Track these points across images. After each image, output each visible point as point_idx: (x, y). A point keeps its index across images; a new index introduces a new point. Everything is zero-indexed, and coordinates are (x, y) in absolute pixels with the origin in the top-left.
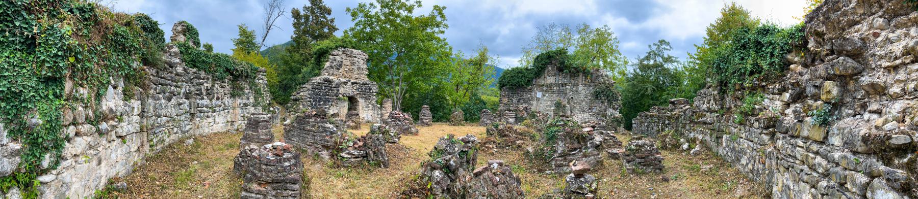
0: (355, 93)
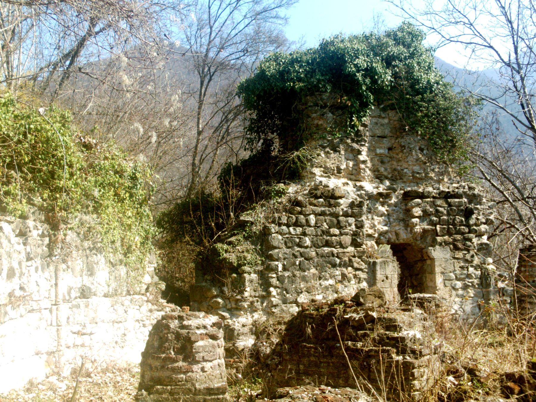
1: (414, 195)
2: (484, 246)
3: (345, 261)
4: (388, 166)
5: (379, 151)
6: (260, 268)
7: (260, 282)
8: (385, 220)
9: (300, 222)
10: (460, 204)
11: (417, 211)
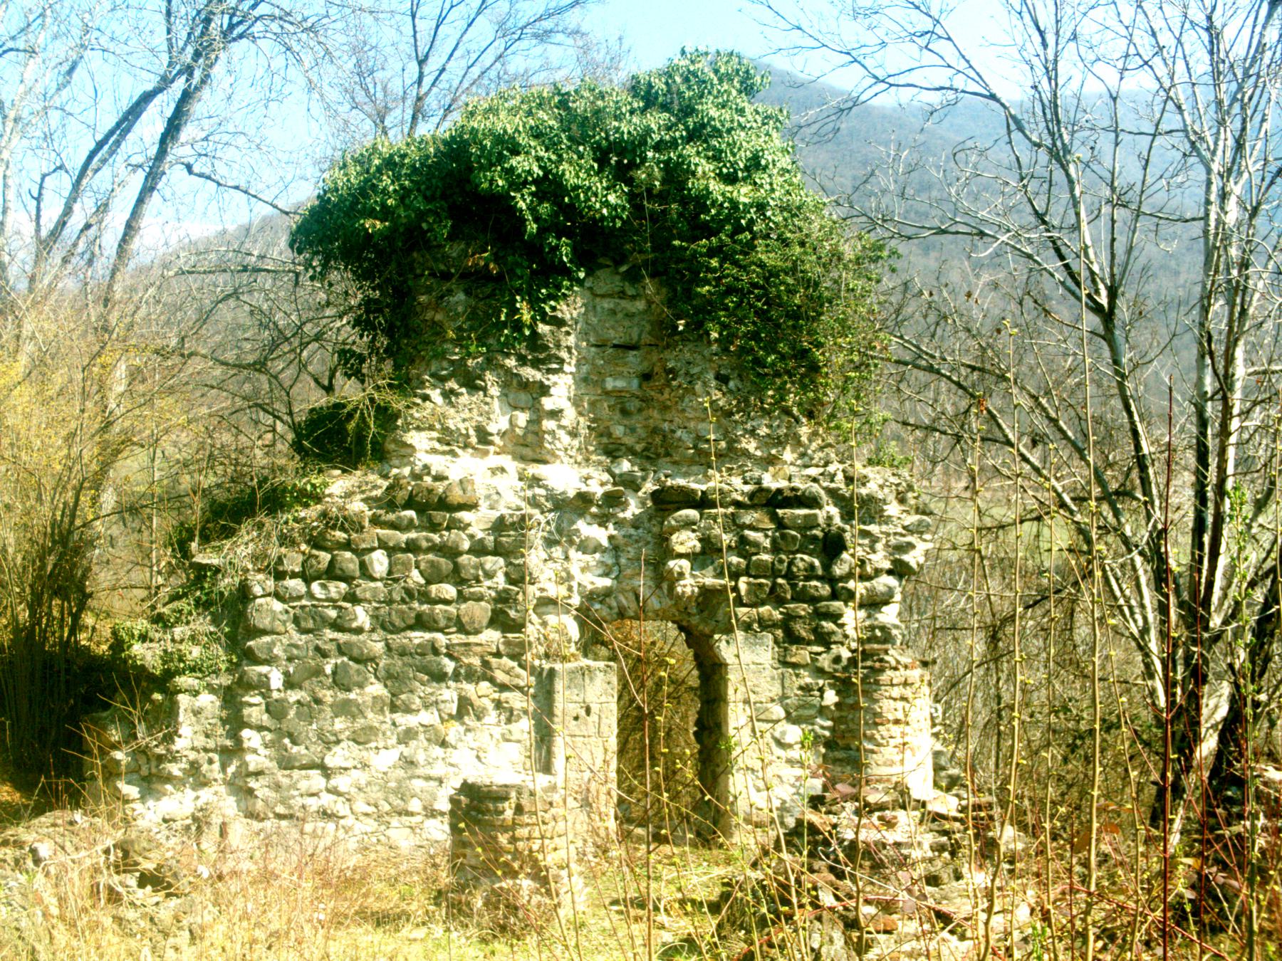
1: (675, 498)
2: (878, 633)
3: (469, 666)
4: (637, 422)
5: (610, 384)
6: (225, 680)
7: (224, 714)
8: (602, 563)
9: (341, 569)
10: (810, 523)
11: (685, 541)
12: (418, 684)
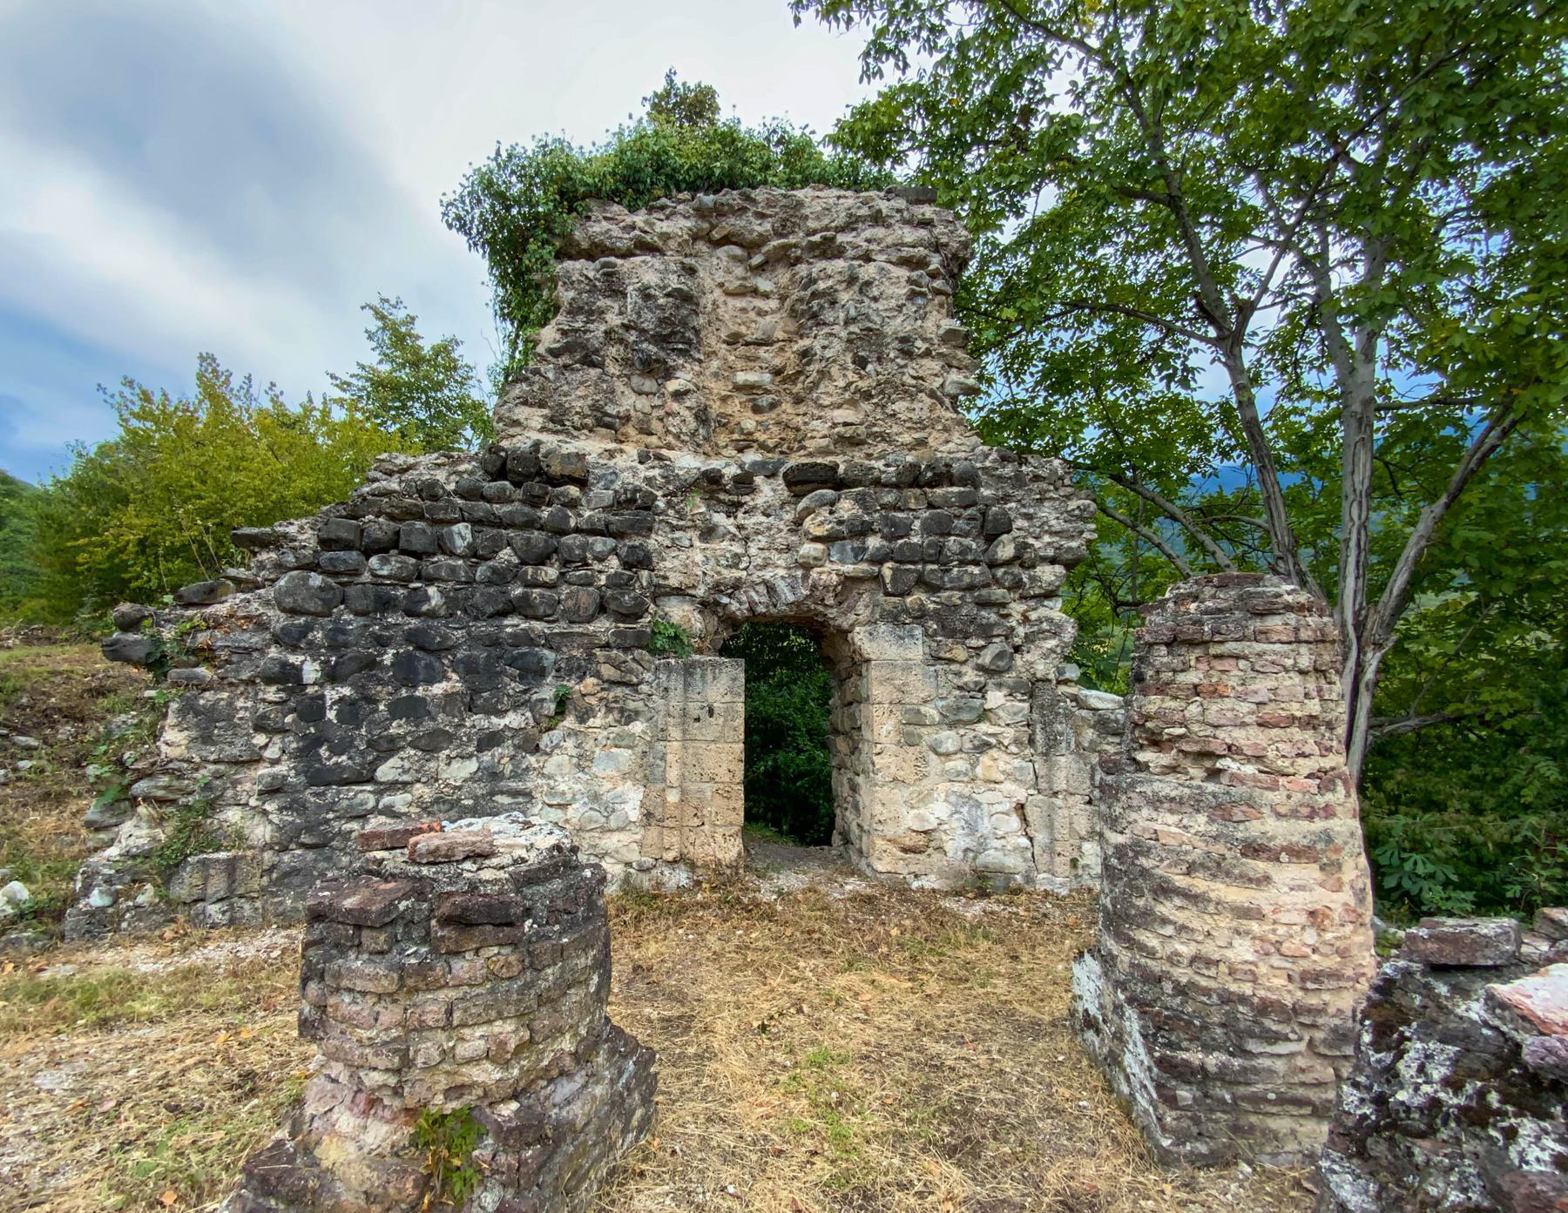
0: (828, 573)
12: (507, 680)
